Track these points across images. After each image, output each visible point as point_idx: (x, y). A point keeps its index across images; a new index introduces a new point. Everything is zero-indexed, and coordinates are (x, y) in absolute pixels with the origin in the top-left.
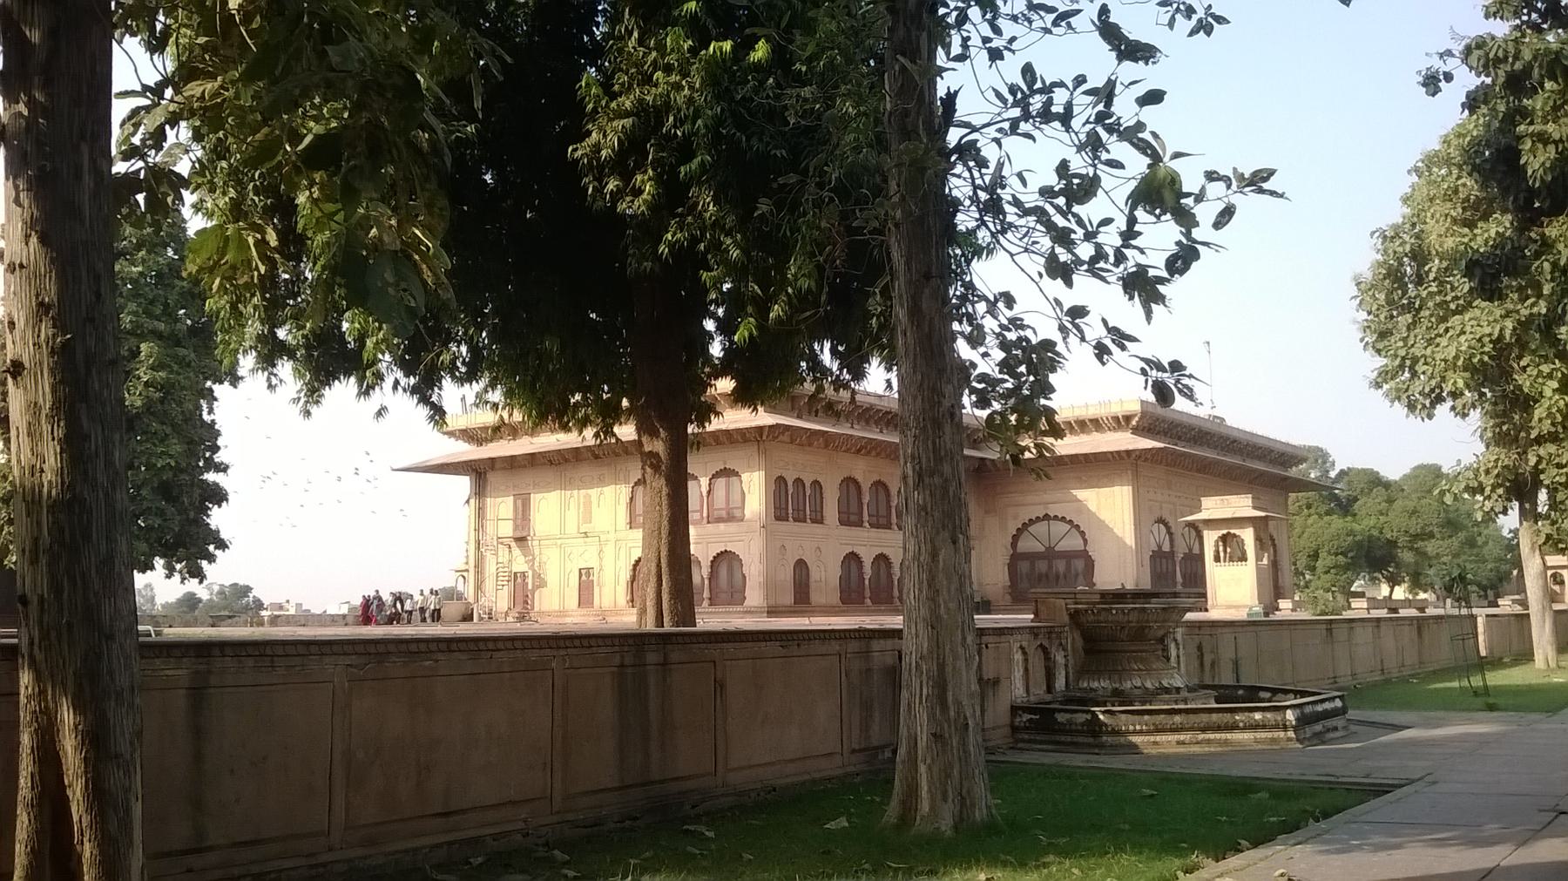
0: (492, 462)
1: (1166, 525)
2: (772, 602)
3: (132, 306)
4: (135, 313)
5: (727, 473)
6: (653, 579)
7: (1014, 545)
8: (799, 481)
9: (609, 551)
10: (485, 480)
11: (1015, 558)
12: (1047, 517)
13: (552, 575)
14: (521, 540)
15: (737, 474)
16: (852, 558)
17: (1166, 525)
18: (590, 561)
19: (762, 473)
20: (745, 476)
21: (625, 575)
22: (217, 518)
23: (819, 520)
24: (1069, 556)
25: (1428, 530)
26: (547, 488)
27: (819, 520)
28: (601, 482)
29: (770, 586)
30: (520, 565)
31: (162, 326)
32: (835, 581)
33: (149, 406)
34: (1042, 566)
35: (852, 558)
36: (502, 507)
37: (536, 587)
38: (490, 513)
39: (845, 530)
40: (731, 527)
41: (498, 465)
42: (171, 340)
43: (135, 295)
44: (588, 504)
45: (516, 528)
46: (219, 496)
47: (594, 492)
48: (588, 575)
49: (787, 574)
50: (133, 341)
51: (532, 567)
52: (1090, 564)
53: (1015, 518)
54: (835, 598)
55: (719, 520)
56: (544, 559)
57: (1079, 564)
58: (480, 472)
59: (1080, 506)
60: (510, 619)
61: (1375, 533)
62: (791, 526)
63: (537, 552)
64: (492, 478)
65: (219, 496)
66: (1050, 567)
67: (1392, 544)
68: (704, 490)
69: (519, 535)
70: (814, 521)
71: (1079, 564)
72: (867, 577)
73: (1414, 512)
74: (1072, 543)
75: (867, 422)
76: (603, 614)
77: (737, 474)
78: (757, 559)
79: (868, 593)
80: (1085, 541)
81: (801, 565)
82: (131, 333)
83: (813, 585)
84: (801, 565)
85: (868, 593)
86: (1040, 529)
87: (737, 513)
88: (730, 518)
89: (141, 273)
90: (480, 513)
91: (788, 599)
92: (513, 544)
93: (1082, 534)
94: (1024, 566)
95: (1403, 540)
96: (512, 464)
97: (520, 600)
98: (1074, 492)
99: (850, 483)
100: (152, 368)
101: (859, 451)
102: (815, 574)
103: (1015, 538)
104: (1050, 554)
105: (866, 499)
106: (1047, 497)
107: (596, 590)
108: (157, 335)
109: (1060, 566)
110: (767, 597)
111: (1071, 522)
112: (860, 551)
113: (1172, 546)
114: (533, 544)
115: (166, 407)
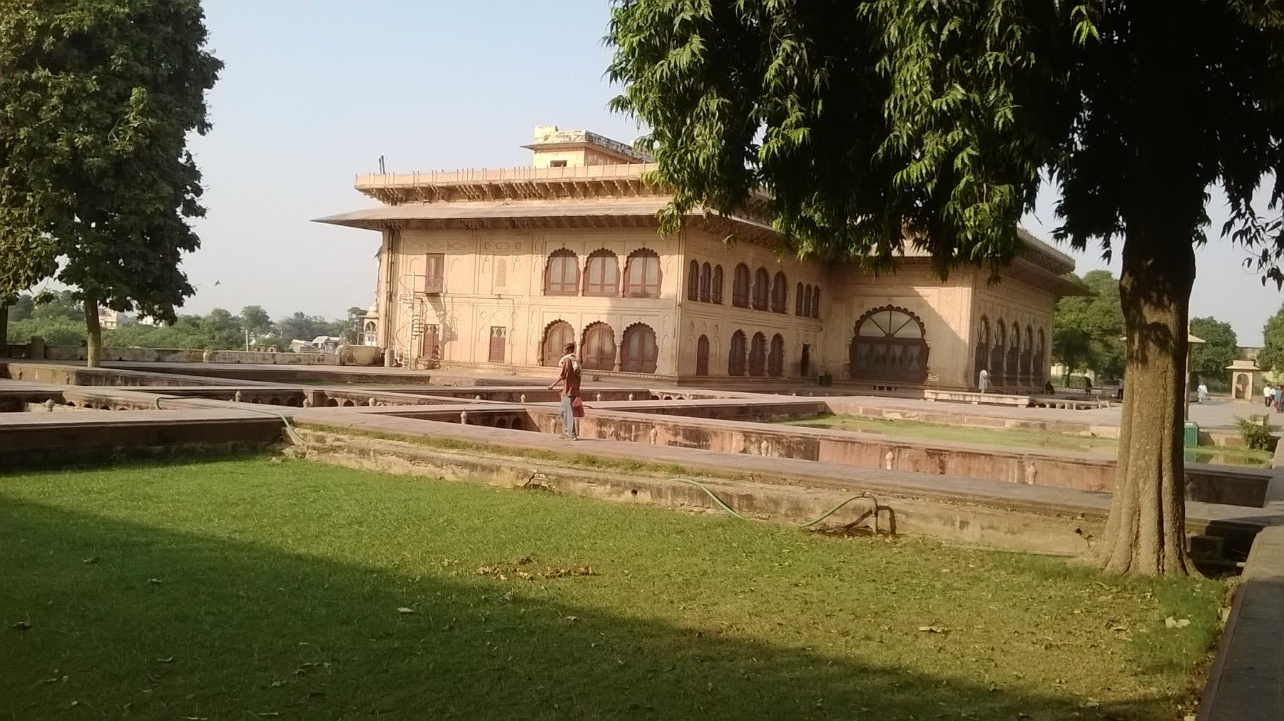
0: (407, 223)
1: (987, 323)
2: (682, 373)
3: (122, 48)
4: (124, 56)
5: (646, 253)
6: (1153, 476)
7: (857, 329)
8: (707, 265)
9: (522, 314)
10: (399, 238)
11: (857, 342)
12: (890, 308)
13: (462, 330)
14: (433, 296)
15: (655, 255)
16: (739, 335)
17: (987, 323)
18: (502, 319)
19: (682, 257)
20: (663, 258)
21: (538, 336)
22: (187, 263)
23: (718, 301)
24: (907, 342)
25: (1117, 326)
26: (462, 250)
27: (718, 301)
28: (518, 250)
29: (681, 358)
30: (432, 318)
31: (147, 70)
32: (726, 356)
33: (137, 154)
34: (881, 349)
35: (739, 335)
36: (414, 266)
37: (445, 340)
38: (401, 269)
39: (737, 311)
40: (646, 303)
41: (412, 225)
42: (154, 86)
43: (123, 37)
44: (503, 266)
45: (428, 284)
46: (192, 243)
47: (509, 259)
48: (499, 332)
49: (693, 347)
50: (121, 84)
51: (443, 321)
52: (925, 350)
53: (862, 306)
54: (725, 372)
55: (636, 295)
56: (456, 314)
57: (915, 351)
58: (394, 232)
59: (923, 304)
60: (420, 366)
61: (1075, 326)
62: (698, 306)
63: (449, 308)
64: (404, 235)
65: (192, 243)
66: (888, 349)
67: (1087, 336)
68: (622, 266)
69: (431, 291)
70: (775, 310)
71: (915, 351)
72: (767, 354)
73: (1108, 312)
74: (912, 332)
75: (760, 214)
76: (514, 369)
77: (655, 255)
78: (671, 334)
79: (766, 366)
80: (923, 332)
81: (703, 340)
82: (121, 75)
83: (710, 358)
84: (703, 340)
85: (766, 366)
86: (883, 317)
87: (650, 290)
88: (645, 295)
89: (128, 15)
90: (392, 266)
91: (692, 370)
92: (425, 299)
93: (921, 325)
94: (864, 349)
95: (1096, 333)
96: (428, 226)
97: (430, 349)
98: (918, 289)
99: (742, 268)
100: (141, 113)
101: (752, 241)
102: (712, 349)
103: (859, 324)
104: (890, 340)
105: (753, 283)
106: (892, 291)
107: (508, 347)
108: (143, 81)
109: (898, 350)
110: (678, 368)
111: (912, 314)
112: (745, 329)
113: (987, 339)
114: (446, 300)
115: (154, 153)
